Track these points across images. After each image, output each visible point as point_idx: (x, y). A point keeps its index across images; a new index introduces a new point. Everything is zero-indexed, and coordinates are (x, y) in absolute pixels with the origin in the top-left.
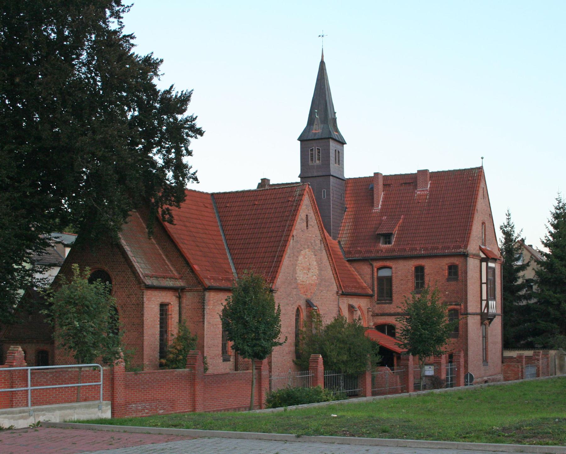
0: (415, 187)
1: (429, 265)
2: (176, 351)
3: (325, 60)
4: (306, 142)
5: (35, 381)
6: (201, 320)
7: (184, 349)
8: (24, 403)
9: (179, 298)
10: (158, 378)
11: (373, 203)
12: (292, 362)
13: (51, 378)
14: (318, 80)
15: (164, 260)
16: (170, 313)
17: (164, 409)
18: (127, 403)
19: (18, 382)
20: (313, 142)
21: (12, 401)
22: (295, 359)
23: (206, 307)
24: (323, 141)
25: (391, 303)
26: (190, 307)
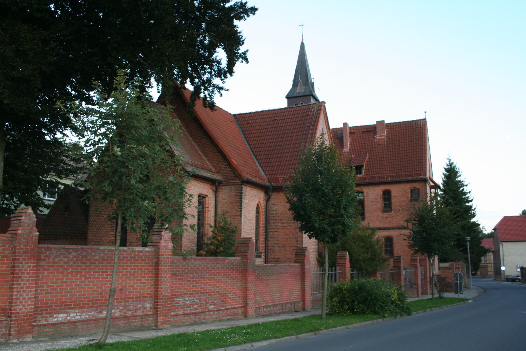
0: (375, 133)
1: (396, 190)
2: (217, 242)
3: (304, 42)
4: (292, 99)
5: (51, 260)
6: (239, 213)
7: (224, 241)
8: (30, 291)
9: (216, 192)
10: (209, 266)
11: (343, 145)
12: (316, 260)
13: (74, 257)
14: (299, 55)
15: (200, 155)
16: (207, 206)
17: (214, 305)
18: (174, 296)
19: (23, 259)
20: (298, 99)
21: (12, 288)
22: (318, 257)
23: (243, 201)
24: (306, 97)
25: (391, 211)
26: (226, 201)
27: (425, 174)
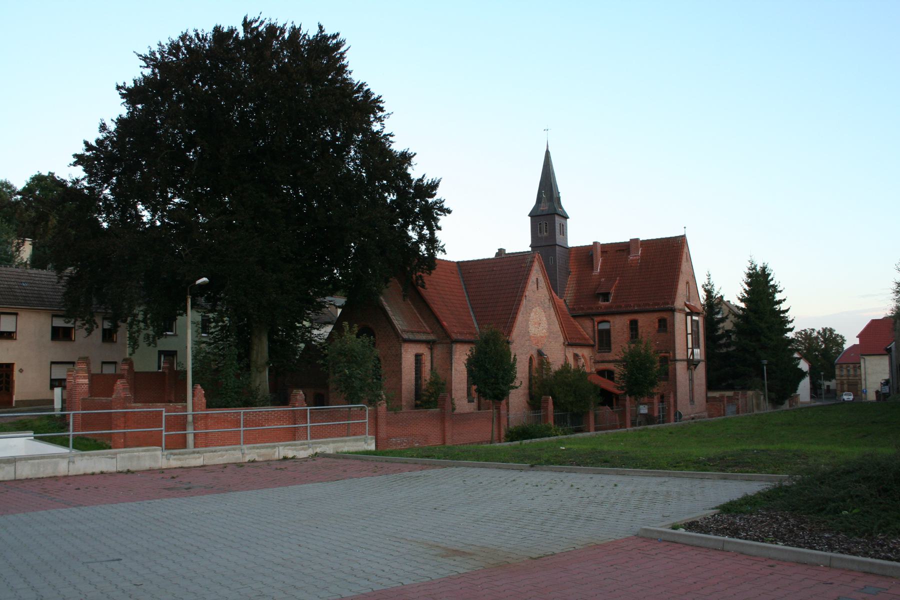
0: (629, 253)
1: (642, 319)
9: (431, 349)
27: (673, 303)
